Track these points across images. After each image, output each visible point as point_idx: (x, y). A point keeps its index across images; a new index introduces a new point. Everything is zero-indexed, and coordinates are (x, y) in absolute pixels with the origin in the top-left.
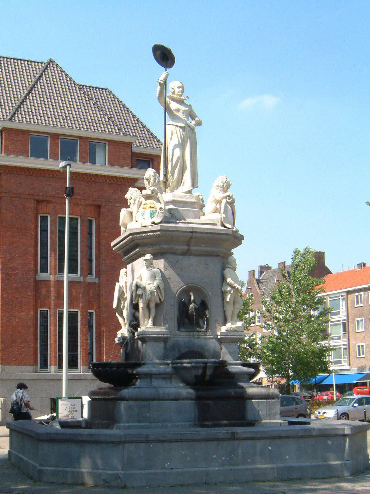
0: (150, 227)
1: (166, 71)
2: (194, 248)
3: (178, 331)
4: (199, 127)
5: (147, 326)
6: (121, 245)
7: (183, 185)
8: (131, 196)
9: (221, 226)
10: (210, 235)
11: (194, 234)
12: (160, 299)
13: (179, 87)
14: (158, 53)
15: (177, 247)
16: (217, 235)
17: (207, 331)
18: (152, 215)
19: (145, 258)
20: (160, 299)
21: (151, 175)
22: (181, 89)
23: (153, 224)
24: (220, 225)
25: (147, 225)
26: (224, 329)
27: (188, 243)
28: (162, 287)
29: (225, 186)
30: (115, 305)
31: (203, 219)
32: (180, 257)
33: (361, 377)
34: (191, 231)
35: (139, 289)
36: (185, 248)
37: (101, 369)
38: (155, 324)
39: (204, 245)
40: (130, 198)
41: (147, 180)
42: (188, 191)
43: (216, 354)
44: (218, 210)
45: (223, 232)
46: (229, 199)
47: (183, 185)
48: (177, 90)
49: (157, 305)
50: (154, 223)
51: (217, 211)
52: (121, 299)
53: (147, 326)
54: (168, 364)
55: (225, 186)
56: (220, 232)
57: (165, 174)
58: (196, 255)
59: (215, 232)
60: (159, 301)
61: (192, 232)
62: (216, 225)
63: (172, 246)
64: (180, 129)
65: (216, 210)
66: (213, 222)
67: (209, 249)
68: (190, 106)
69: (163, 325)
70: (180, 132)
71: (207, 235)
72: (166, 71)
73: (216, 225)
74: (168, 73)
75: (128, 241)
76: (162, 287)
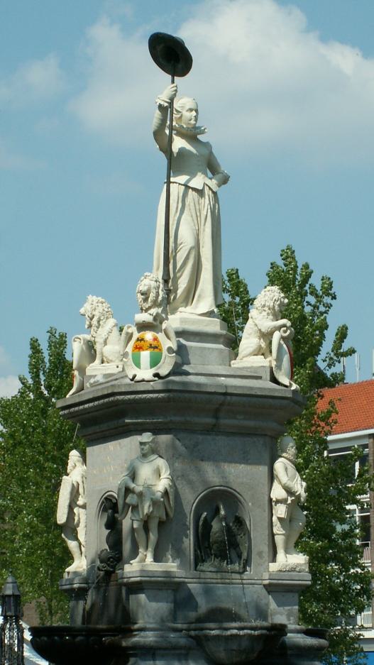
0: (152, 383)
1: (173, 82)
2: (225, 422)
3: (196, 570)
4: (225, 185)
5: (140, 565)
6: (85, 409)
7: (198, 300)
8: (94, 313)
9: (271, 381)
10: (254, 400)
11: (229, 398)
12: (167, 514)
13: (191, 110)
14: (160, 48)
15: (197, 420)
16: (265, 400)
17: (244, 572)
18: (155, 362)
19: (139, 438)
20: (167, 514)
21: (152, 286)
22: (194, 113)
23: (156, 379)
24: (269, 378)
25: (146, 379)
26: (273, 567)
27: (216, 413)
28: (171, 492)
29: (276, 307)
30: (61, 517)
31: (236, 364)
32: (200, 437)
33: (184, 503)
34: (224, 391)
35: (130, 495)
36: (209, 420)
37: (45, 639)
38: (157, 558)
39: (242, 417)
40: (91, 316)
41: (142, 294)
42: (208, 312)
43: (262, 613)
44: (262, 351)
45: (276, 394)
46: (285, 332)
47: (198, 300)
48: (187, 115)
49: (161, 524)
50: (156, 375)
51: (265, 352)
52: (73, 506)
53: (140, 565)
54: (181, 630)
55: (276, 307)
56: (272, 394)
57: (166, 278)
58: (228, 434)
59: (264, 394)
60: (165, 517)
61: (225, 394)
62: (260, 378)
63: (188, 419)
64: (194, 192)
65: (260, 349)
66: (255, 373)
67: (251, 423)
68: (207, 145)
69: (171, 559)
70: (194, 200)
71: (249, 399)
72: (173, 82)
73: (260, 378)
74: (176, 86)
75: (103, 404)
76: (171, 492)
